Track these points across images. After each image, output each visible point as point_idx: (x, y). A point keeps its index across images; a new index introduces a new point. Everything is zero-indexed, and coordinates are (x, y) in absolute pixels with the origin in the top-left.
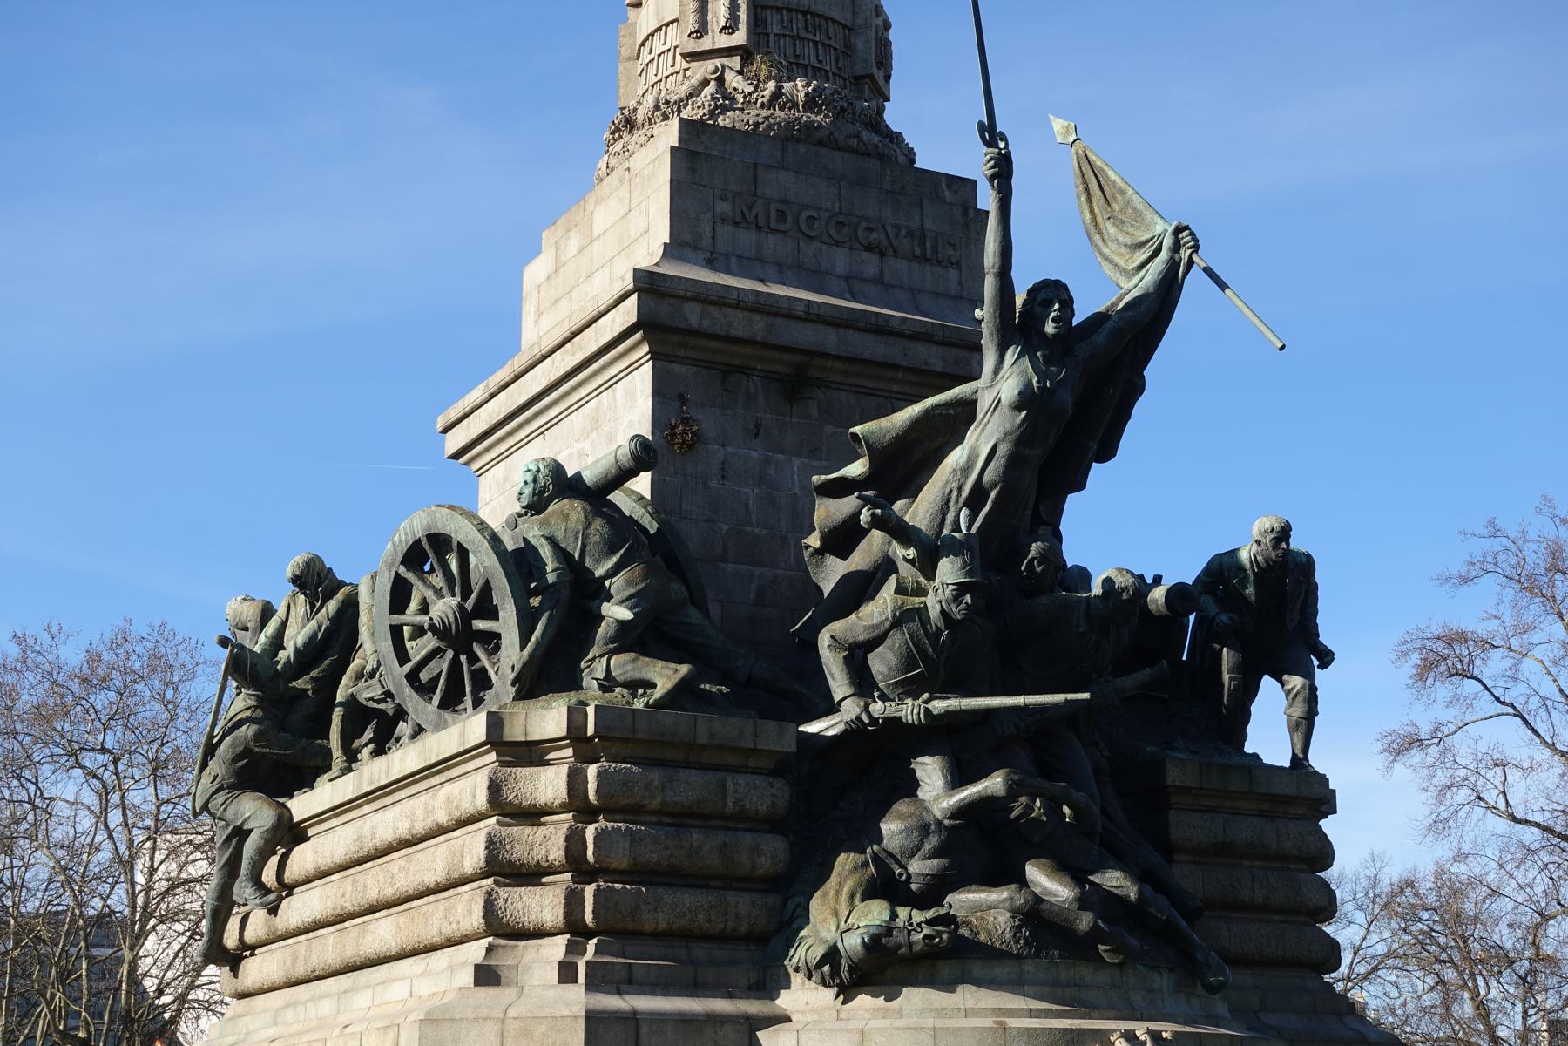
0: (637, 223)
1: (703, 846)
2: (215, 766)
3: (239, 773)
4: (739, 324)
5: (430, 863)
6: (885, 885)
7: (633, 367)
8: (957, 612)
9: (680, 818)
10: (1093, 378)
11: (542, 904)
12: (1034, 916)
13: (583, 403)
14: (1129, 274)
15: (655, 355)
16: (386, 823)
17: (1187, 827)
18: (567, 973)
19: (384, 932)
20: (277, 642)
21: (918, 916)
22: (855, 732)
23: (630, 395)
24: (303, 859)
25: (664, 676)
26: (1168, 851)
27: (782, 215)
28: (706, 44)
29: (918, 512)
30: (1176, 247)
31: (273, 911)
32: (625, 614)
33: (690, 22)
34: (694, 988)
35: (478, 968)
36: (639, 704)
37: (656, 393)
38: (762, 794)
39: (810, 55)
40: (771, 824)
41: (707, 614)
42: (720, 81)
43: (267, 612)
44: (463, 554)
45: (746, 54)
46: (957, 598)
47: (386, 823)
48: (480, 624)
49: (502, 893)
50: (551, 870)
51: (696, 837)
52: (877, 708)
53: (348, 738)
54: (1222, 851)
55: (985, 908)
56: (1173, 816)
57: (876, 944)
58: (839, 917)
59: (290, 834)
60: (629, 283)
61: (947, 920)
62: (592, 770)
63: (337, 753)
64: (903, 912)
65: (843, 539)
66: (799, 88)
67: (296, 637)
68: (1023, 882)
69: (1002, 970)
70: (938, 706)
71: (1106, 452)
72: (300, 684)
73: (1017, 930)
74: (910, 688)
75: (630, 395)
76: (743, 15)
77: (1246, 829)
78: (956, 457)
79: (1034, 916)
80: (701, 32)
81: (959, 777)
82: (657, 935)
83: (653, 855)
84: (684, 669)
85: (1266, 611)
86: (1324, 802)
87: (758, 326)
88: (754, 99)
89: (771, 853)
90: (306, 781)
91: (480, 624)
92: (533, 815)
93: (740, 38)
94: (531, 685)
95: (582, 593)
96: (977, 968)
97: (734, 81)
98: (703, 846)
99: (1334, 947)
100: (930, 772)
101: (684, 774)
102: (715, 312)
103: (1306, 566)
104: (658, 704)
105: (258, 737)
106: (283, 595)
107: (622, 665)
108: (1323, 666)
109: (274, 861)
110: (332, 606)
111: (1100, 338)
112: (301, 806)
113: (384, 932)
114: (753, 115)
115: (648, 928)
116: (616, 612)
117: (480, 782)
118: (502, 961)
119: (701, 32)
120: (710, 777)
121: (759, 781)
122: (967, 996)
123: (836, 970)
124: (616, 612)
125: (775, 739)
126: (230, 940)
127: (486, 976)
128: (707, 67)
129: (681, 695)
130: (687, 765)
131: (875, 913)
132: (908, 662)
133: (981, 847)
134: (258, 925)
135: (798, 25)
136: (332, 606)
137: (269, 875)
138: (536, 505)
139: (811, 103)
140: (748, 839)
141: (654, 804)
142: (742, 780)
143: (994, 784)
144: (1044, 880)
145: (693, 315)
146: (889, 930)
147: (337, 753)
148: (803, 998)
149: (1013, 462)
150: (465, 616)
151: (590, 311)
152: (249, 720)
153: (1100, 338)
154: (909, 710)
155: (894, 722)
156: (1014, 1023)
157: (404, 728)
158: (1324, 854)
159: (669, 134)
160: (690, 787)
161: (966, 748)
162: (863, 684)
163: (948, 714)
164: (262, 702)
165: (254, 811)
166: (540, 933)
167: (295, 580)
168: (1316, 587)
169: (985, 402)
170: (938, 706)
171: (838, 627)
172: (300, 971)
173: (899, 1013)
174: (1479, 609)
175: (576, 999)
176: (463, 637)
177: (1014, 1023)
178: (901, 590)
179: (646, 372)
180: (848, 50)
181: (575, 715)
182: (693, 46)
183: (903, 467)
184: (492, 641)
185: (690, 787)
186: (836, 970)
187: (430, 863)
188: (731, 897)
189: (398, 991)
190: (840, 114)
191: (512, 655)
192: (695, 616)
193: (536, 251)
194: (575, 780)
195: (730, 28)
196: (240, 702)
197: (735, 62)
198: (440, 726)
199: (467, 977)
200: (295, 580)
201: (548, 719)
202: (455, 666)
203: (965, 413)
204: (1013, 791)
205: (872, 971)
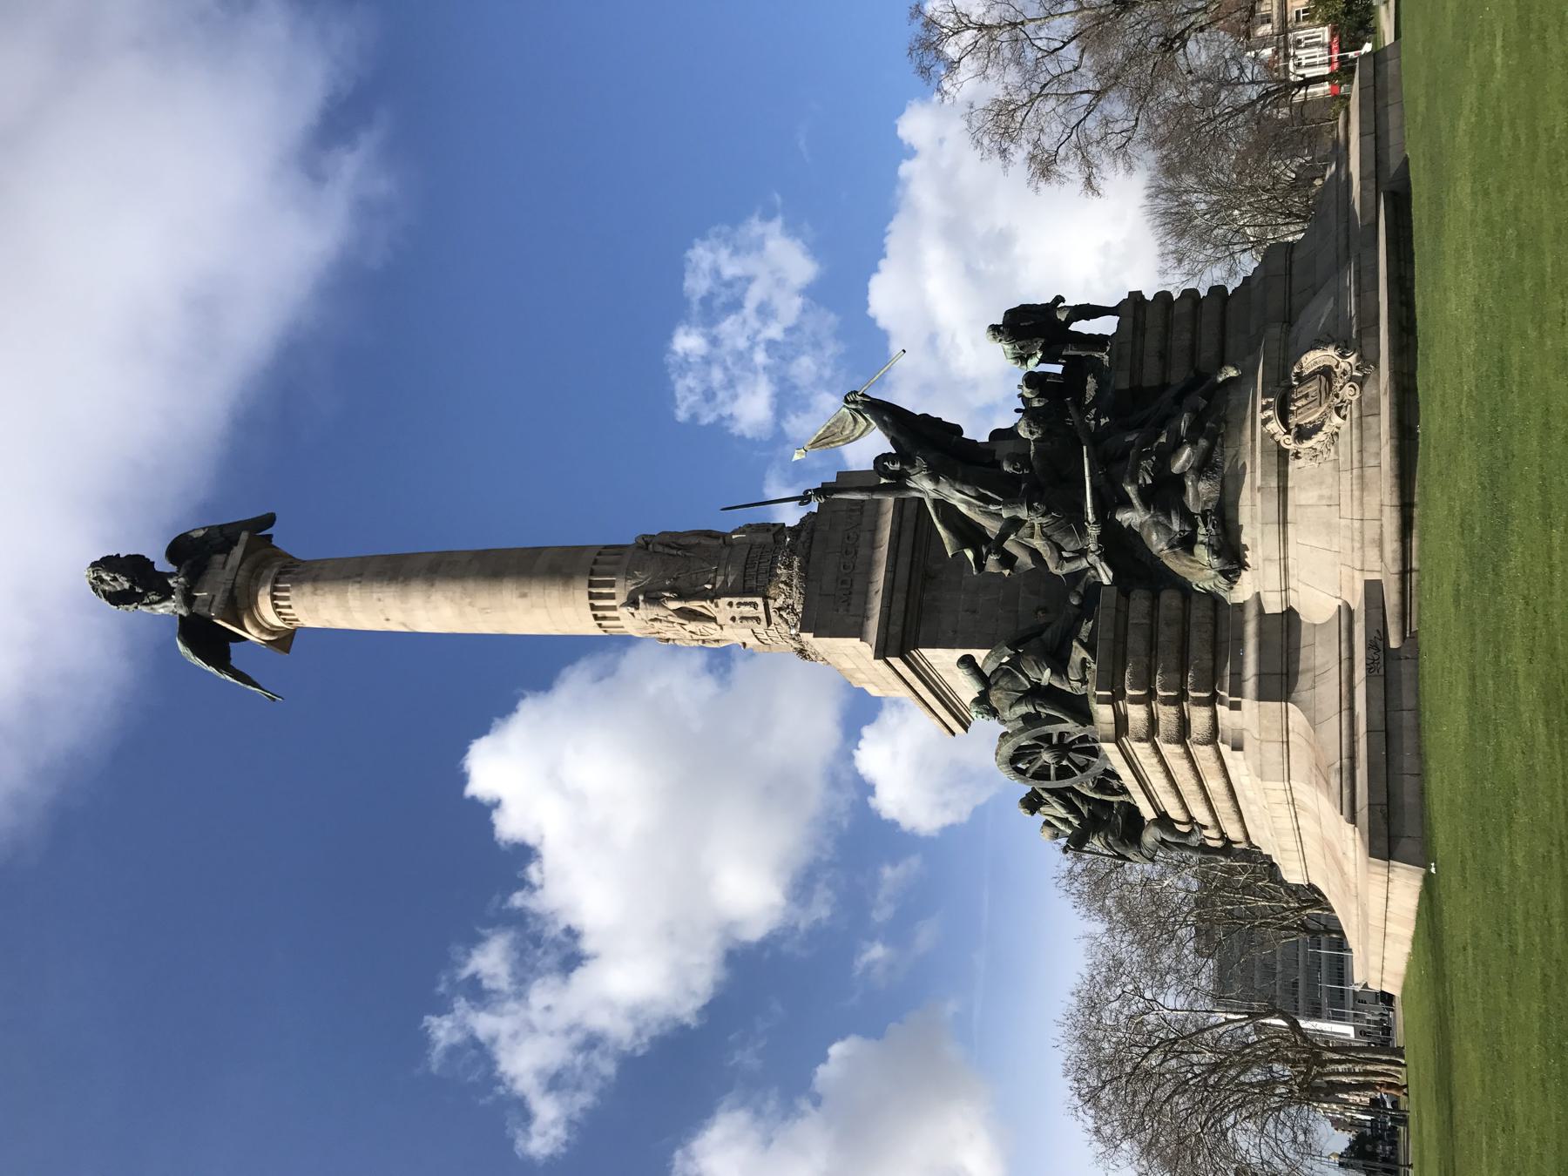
0: (850, 651)
1: (1167, 635)
2: (1130, 855)
3: (1132, 843)
4: (899, 606)
5: (1180, 768)
6: (1186, 544)
7: (921, 656)
8: (1042, 508)
9: (1152, 646)
10: (923, 439)
11: (1199, 718)
12: (1204, 467)
13: (939, 676)
14: (869, 424)
15: (916, 647)
16: (1157, 781)
17: (1151, 374)
18: (1235, 706)
19: (1215, 784)
20: (1065, 821)
21: (1202, 530)
22: (1106, 557)
23: (934, 657)
24: (1175, 813)
25: (1078, 654)
26: (1165, 386)
27: (843, 582)
28: (763, 616)
29: (992, 527)
30: (855, 402)
31: (1205, 827)
32: (1048, 672)
33: (753, 624)
34: (1240, 641)
35: (1234, 749)
36: (1094, 667)
37: (934, 647)
38: (1139, 603)
39: (765, 566)
40: (1155, 598)
41: (1048, 625)
42: (779, 609)
43: (1048, 824)
44: (1021, 748)
45: (766, 598)
46: (1036, 510)
47: (1157, 781)
48: (1055, 740)
49: (1194, 736)
50: (1182, 711)
51: (1161, 639)
52: (1092, 547)
53: (1115, 793)
54: (1164, 355)
55: (1199, 493)
56: (1145, 384)
57: (1216, 552)
58: (1201, 570)
59: (1163, 820)
60: (881, 662)
61: (1204, 515)
62: (1129, 692)
63: (1121, 798)
64: (1200, 538)
65: (1008, 560)
66: (782, 571)
67: (1061, 812)
68: (1182, 475)
69: (1230, 486)
70: (1091, 517)
71: (957, 430)
72: (1085, 812)
73: (1208, 478)
74: (1082, 532)
75: (934, 657)
76: (748, 600)
77: (1152, 343)
78: (963, 508)
79: (1204, 467)
80: (758, 619)
81: (1127, 504)
82: (1214, 659)
83: (1173, 662)
84: (1075, 644)
85: (1030, 326)
86: (1136, 297)
87: (900, 597)
88: (787, 595)
89: (1169, 599)
90: (1132, 811)
91: (1055, 740)
92: (1153, 722)
93: (759, 601)
94: (1086, 717)
95: (1037, 693)
96: (1229, 499)
97: (779, 603)
98: (1167, 635)
99: (1212, 290)
100: (1126, 517)
101: (1130, 645)
102: (893, 618)
103: (1012, 315)
104: (1094, 658)
105: (1114, 835)
106: (1039, 818)
107: (1074, 674)
108: (1063, 300)
109: (1178, 826)
110: (1045, 795)
111: (902, 440)
112: (1148, 813)
113: (1215, 784)
114: (796, 594)
115: (1211, 664)
116: (1046, 676)
117: (1136, 745)
118: (1228, 735)
119: (758, 619)
120: (1130, 632)
121: (1132, 604)
122: (1244, 517)
123: (1233, 571)
124: (1046, 676)
125: (1108, 600)
126: (1219, 844)
127: (1237, 747)
128: (775, 618)
129: (1090, 647)
130: (1125, 643)
131: (1201, 552)
132: (1069, 532)
133: (1164, 495)
134: (1213, 833)
135: (752, 571)
136: (1045, 795)
137: (1185, 829)
138: (994, 712)
139: (789, 566)
140: (1162, 612)
141: (1146, 660)
142: (1131, 615)
143: (1131, 490)
144: (1183, 460)
145: (895, 629)
146: (1209, 546)
147: (1121, 798)
148: (1243, 591)
149: (964, 482)
150: (1051, 747)
151: (895, 677)
152: (1106, 838)
153: (902, 440)
154: (1093, 531)
155: (1100, 539)
156: (1258, 483)
157: (1132, 954)
158: (1164, 297)
159: (807, 637)
160: (1136, 642)
161: (1111, 500)
162: (1082, 553)
163: (1095, 513)
164: (1096, 831)
165: (1150, 837)
166: (1214, 717)
167: (1032, 813)
168: (1022, 306)
169: (934, 495)
170: (1091, 517)
171: (1052, 567)
172: (1235, 817)
173: (1254, 540)
174: (1020, 153)
175: (1248, 703)
176: (1062, 747)
177: (1258, 483)
178: (1032, 536)
179: (925, 652)
180: (763, 546)
181: (1101, 700)
182: (764, 622)
183: (968, 533)
184: (1061, 735)
185: (1136, 642)
186: (1233, 571)
187: (1180, 768)
188: (1193, 620)
189: (1246, 781)
190: (793, 552)
191: (1071, 727)
192: (1047, 635)
193: (863, 690)
194: (1135, 700)
195: (755, 605)
196: (1096, 843)
197: (771, 602)
198: (1106, 758)
199: (1238, 754)
200: (1032, 813)
201: (1104, 713)
202: (1078, 751)
203: (941, 505)
204: (1134, 481)
205: (1233, 558)
